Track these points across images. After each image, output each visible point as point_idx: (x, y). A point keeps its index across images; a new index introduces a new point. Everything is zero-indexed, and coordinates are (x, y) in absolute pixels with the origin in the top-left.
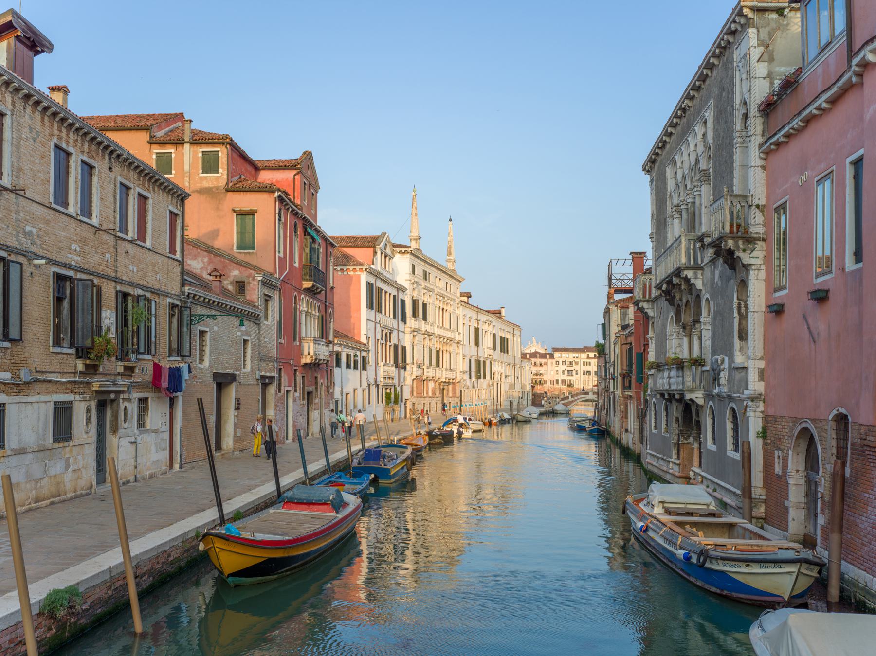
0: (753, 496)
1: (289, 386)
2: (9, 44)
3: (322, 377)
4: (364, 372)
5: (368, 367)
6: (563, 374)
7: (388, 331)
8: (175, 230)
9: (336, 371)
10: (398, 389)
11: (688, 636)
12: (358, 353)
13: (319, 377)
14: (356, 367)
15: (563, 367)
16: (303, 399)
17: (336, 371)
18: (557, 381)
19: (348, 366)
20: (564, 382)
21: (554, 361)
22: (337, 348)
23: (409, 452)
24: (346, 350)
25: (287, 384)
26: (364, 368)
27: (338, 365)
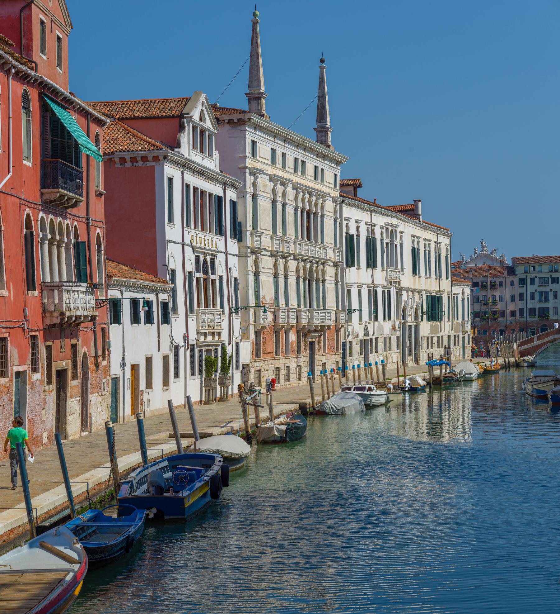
0: (290, 306)
1: (21, 363)
2: (269, 247)
3: (86, 343)
4: (165, 328)
5: (173, 318)
6: (533, 298)
7: (208, 258)
8: (323, 302)
9: (114, 331)
10: (229, 349)
11: (512, 369)
12: (152, 297)
13: (79, 344)
14: (149, 320)
15: (530, 288)
16: (49, 382)
17: (114, 331)
18: (522, 310)
19: (135, 319)
20: (532, 311)
21: (516, 280)
22: (113, 293)
23: (216, 468)
24: (128, 295)
25: (16, 362)
26: (166, 320)
27: (116, 318)
